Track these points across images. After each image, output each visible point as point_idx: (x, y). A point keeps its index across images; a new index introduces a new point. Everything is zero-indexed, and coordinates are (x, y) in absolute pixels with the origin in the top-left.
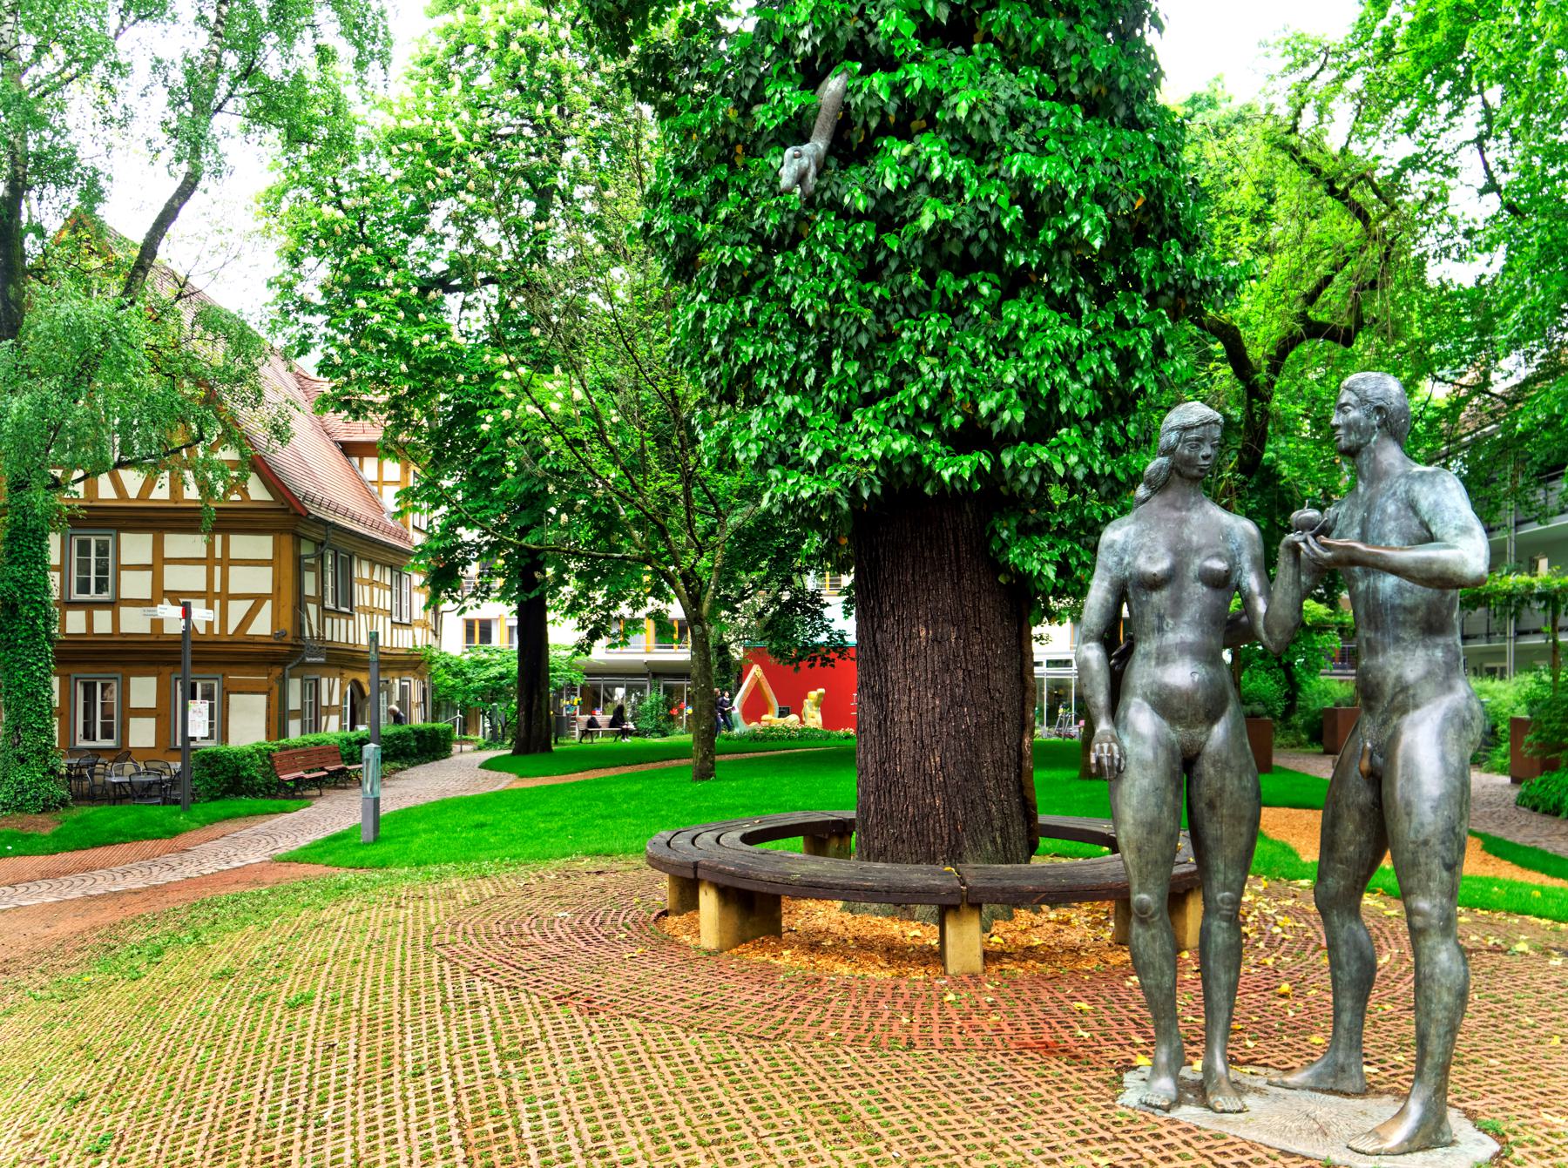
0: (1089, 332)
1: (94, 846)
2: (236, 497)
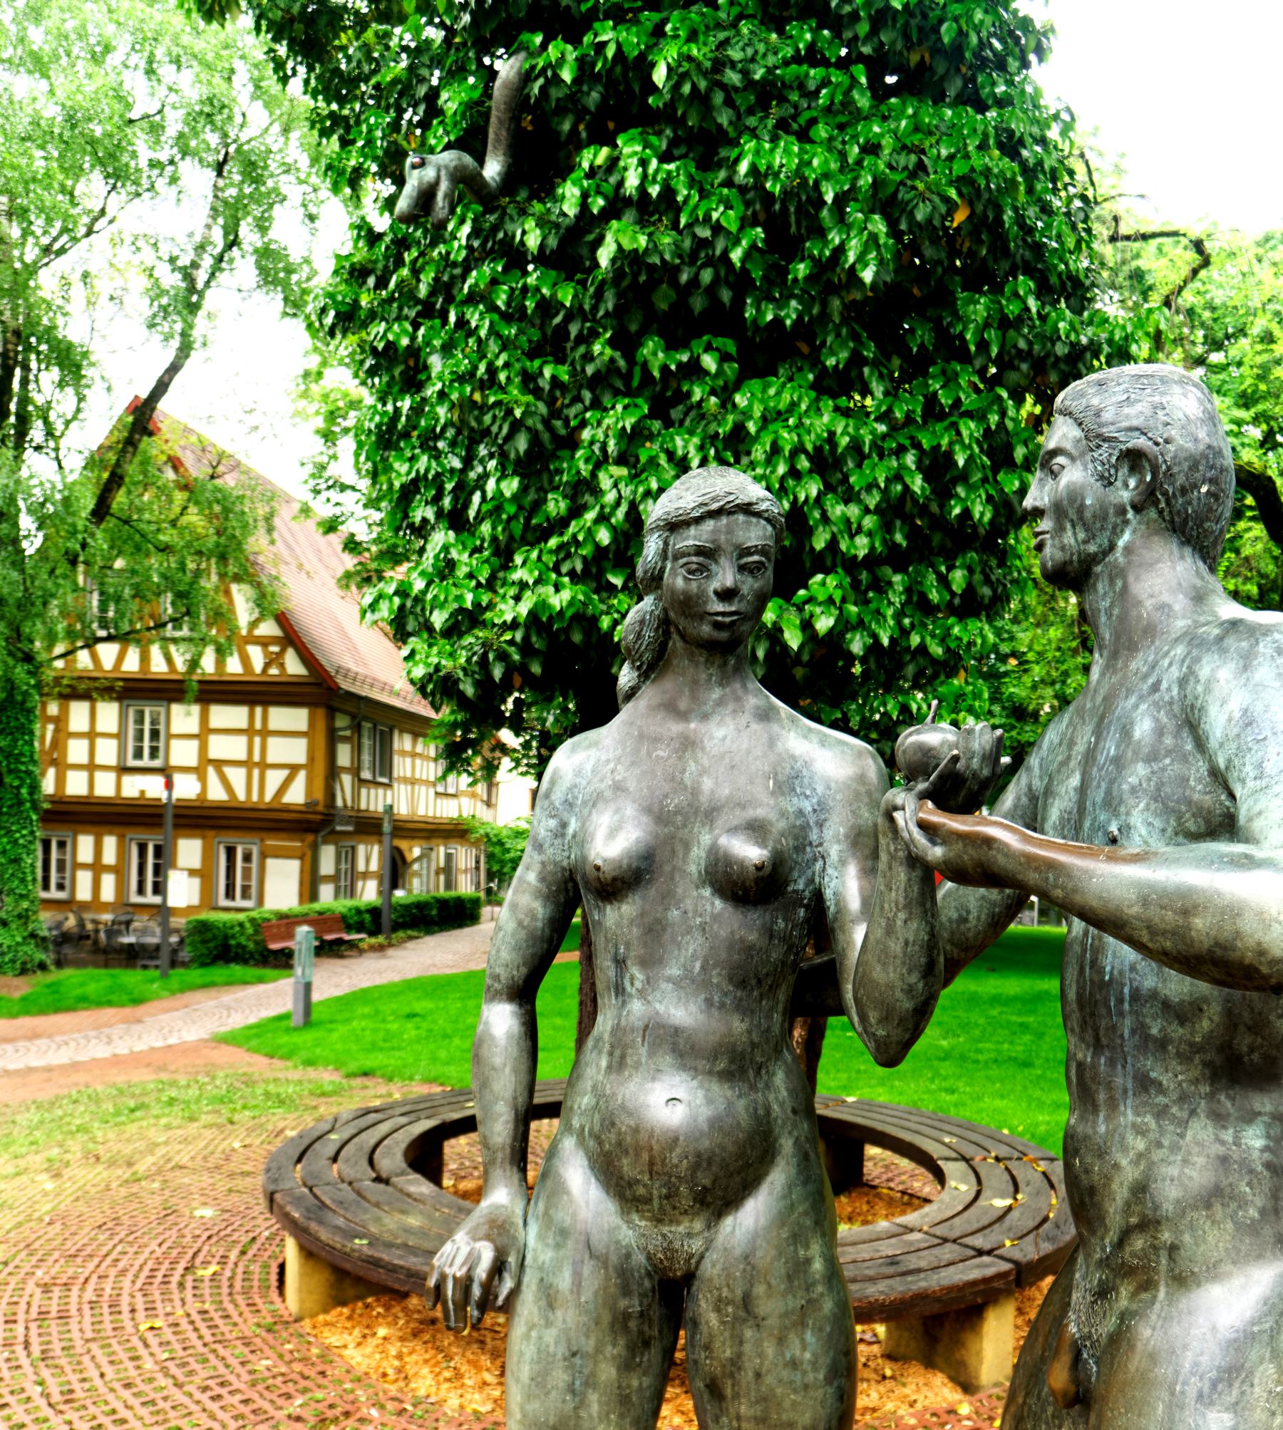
0: (882, 428)
1: (57, 1011)
2: (274, 671)
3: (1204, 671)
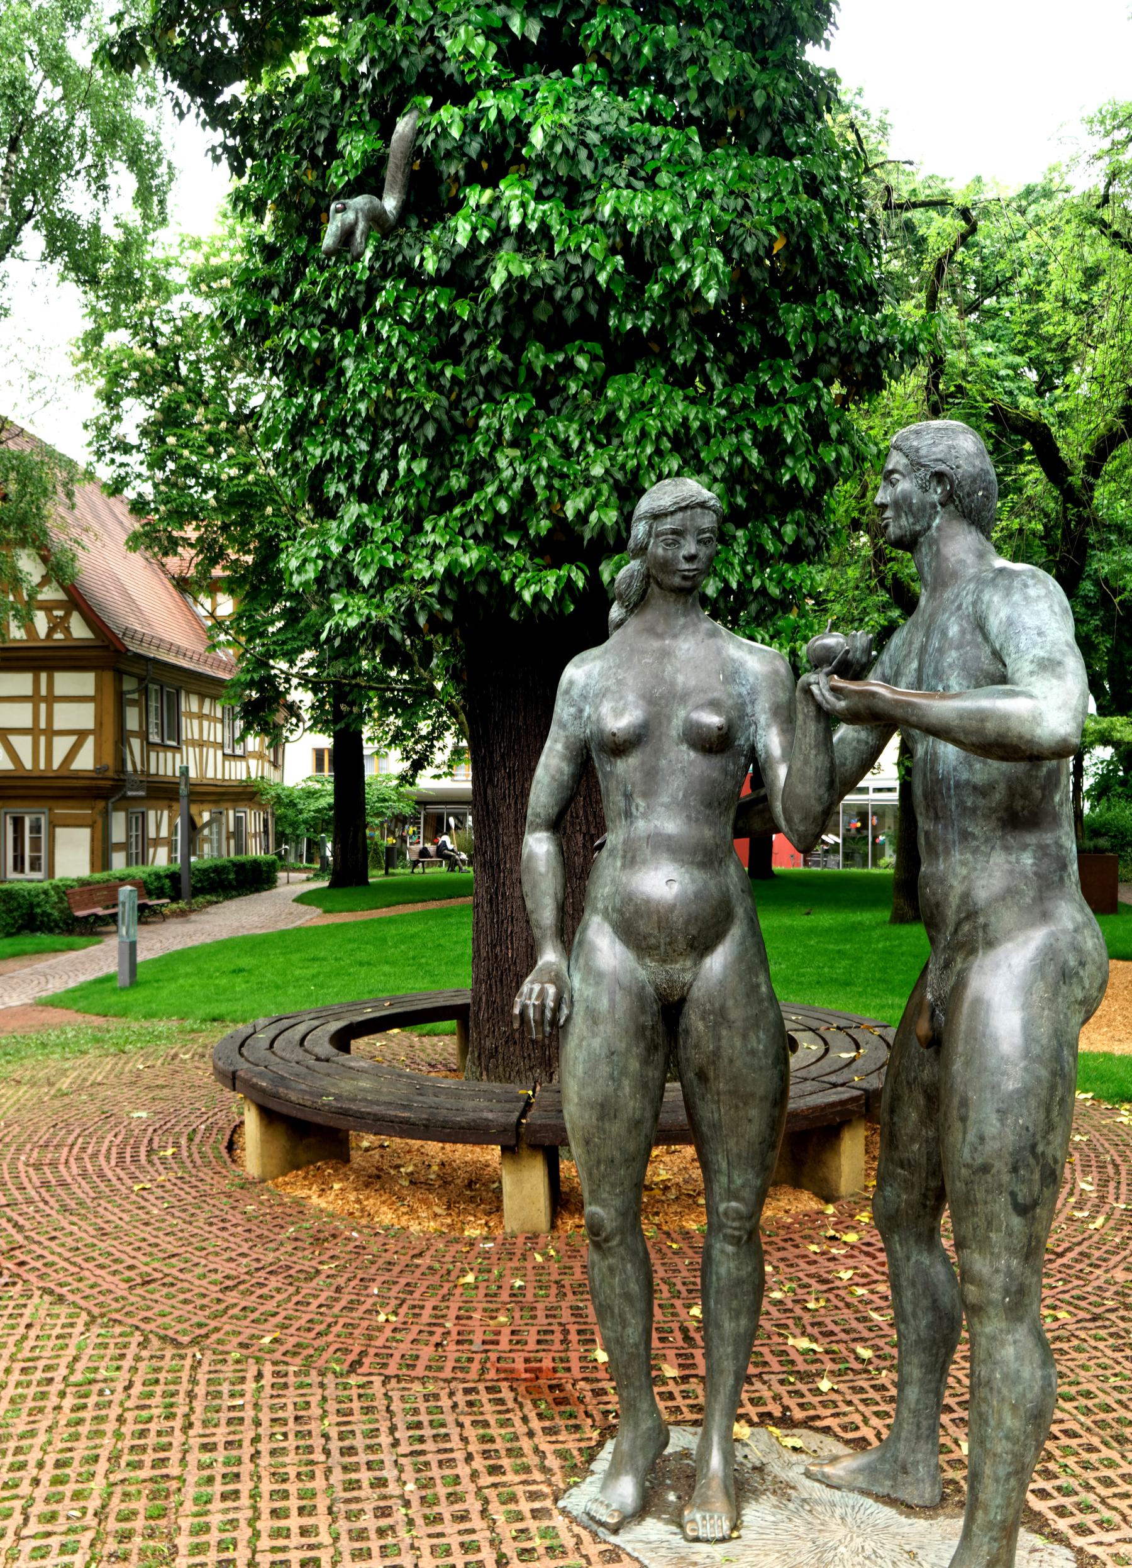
0: (723, 412)
2: (59, 636)
3: (986, 597)
